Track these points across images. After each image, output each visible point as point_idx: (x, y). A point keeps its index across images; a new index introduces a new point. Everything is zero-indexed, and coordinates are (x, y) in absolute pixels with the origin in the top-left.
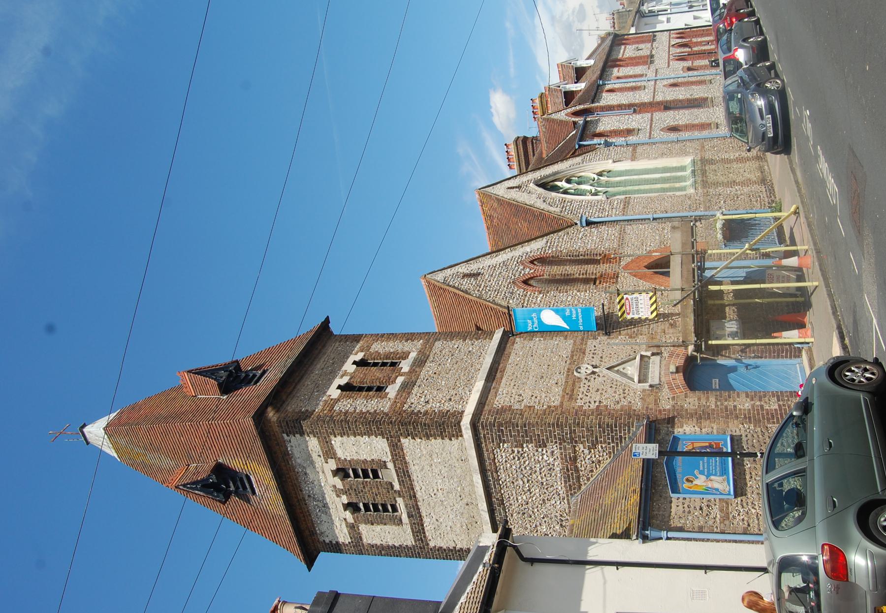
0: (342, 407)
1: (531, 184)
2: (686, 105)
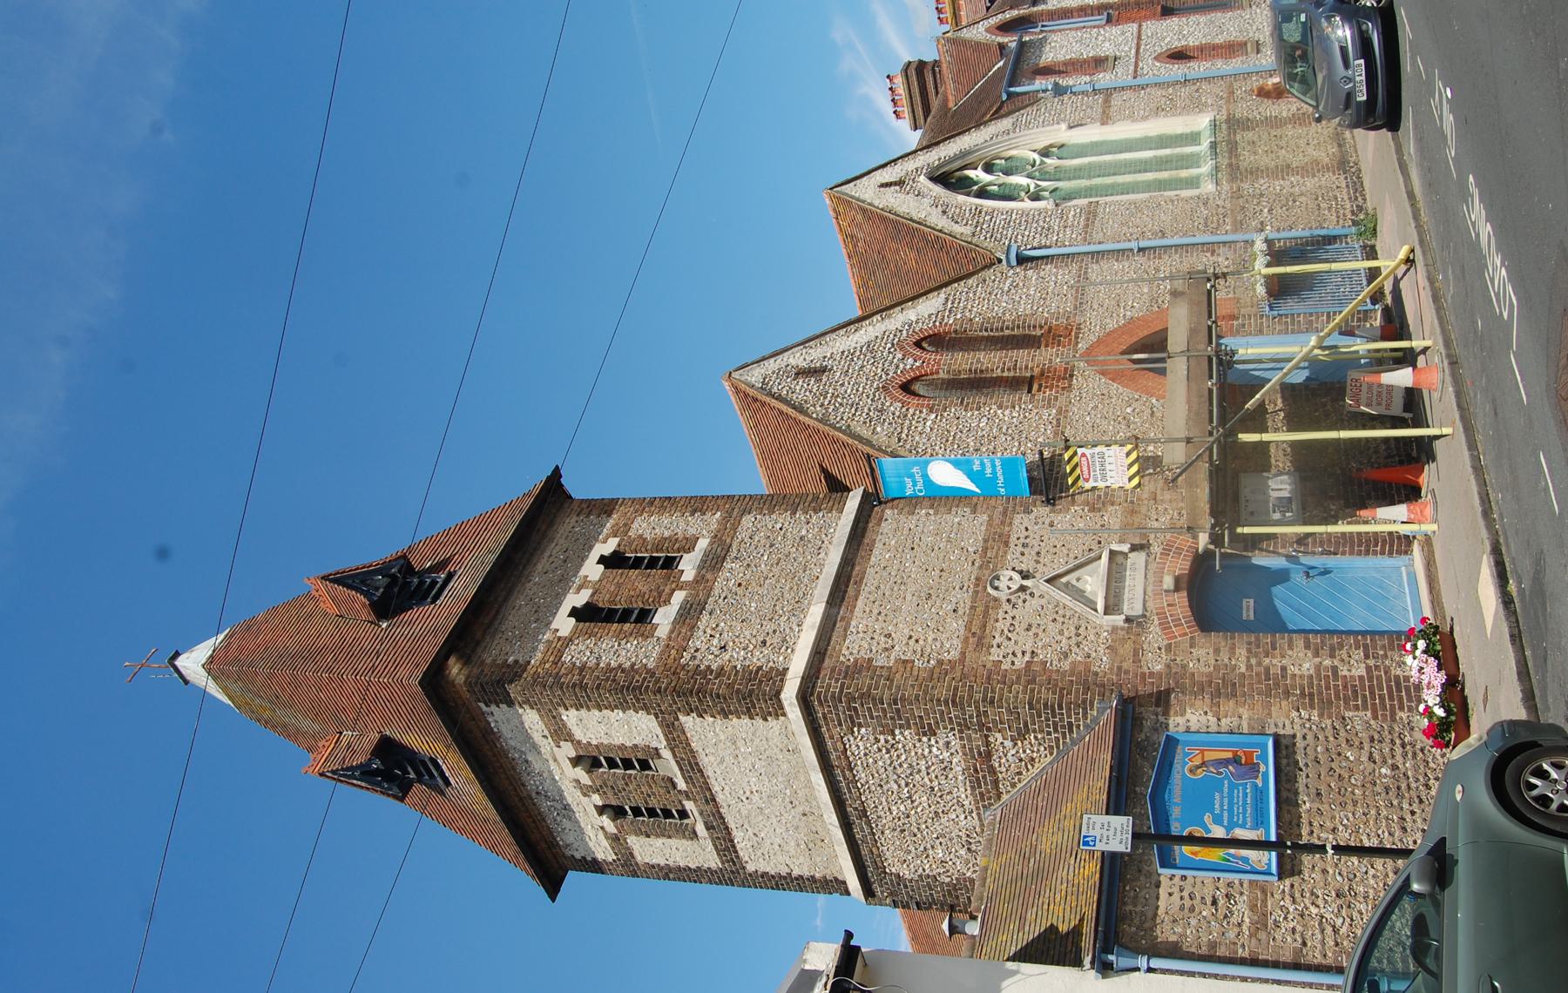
0: (577, 655)
1: (922, 177)
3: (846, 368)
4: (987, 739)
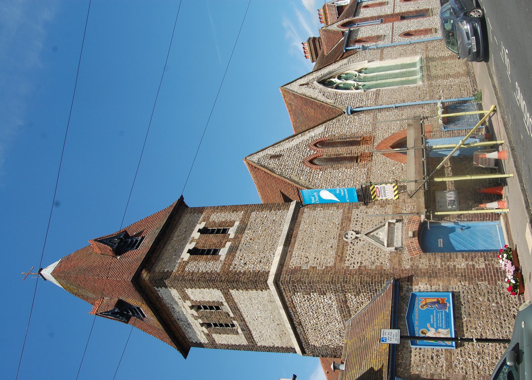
0: (190, 268)
1: (315, 82)
2: (415, 15)
3: (289, 155)
4: (345, 296)
